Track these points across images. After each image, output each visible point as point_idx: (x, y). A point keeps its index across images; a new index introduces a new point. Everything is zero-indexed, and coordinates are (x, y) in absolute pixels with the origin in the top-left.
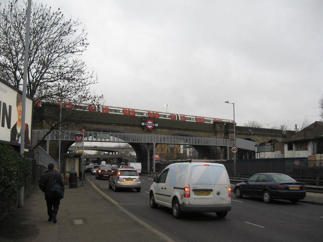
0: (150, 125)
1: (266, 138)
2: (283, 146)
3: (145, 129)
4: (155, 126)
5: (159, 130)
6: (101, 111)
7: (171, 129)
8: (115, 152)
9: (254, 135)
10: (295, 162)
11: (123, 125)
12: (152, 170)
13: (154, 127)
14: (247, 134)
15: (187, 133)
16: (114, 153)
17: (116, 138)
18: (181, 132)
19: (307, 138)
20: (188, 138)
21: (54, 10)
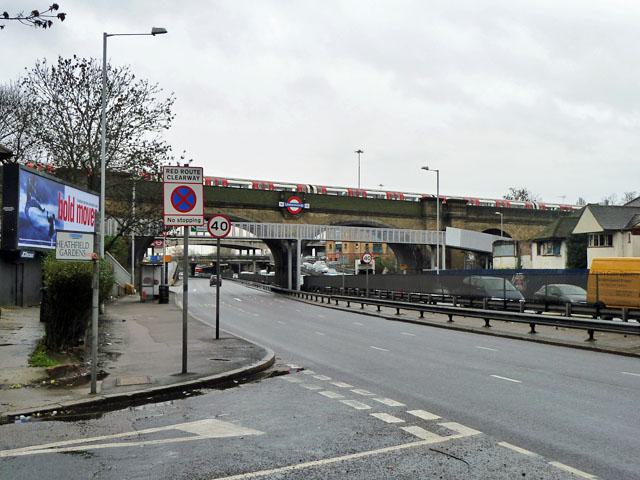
0: (294, 205)
1: (535, 227)
2: (36, 306)
3: (287, 214)
4: (303, 208)
5: (312, 214)
6: (316, 192)
7: (334, 212)
8: (254, 249)
9: (506, 221)
10: (585, 298)
11: (246, 206)
12: (294, 287)
13: (303, 211)
14: (490, 221)
15: (365, 219)
16: (251, 251)
17: (244, 231)
18: (355, 218)
19: (558, 235)
20: (382, 230)
21: (624, 196)
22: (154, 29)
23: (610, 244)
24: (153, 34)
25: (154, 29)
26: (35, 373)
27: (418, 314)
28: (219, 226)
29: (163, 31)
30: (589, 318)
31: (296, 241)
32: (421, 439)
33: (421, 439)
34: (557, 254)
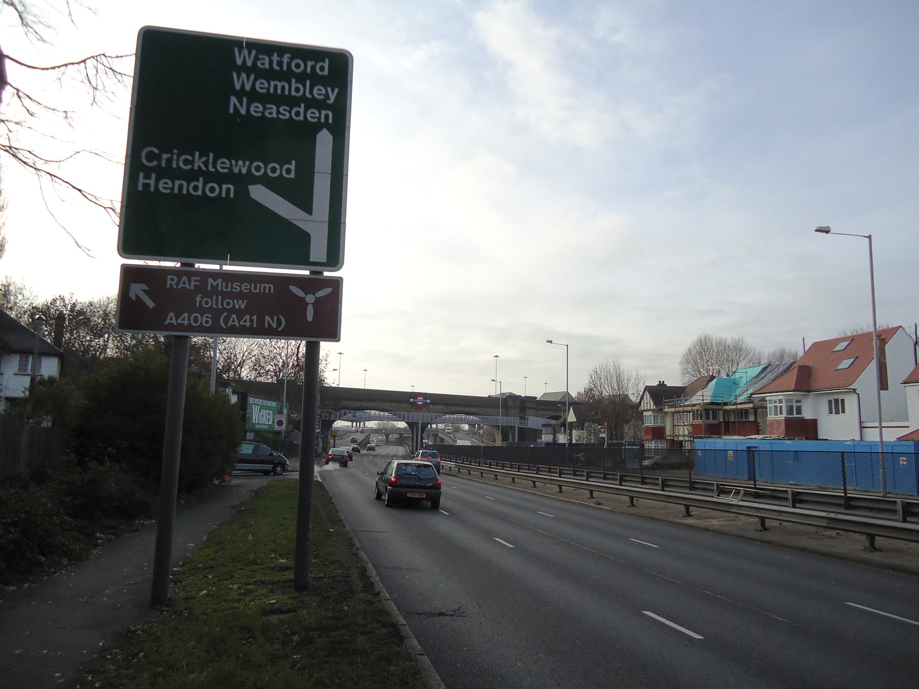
31: (418, 423)
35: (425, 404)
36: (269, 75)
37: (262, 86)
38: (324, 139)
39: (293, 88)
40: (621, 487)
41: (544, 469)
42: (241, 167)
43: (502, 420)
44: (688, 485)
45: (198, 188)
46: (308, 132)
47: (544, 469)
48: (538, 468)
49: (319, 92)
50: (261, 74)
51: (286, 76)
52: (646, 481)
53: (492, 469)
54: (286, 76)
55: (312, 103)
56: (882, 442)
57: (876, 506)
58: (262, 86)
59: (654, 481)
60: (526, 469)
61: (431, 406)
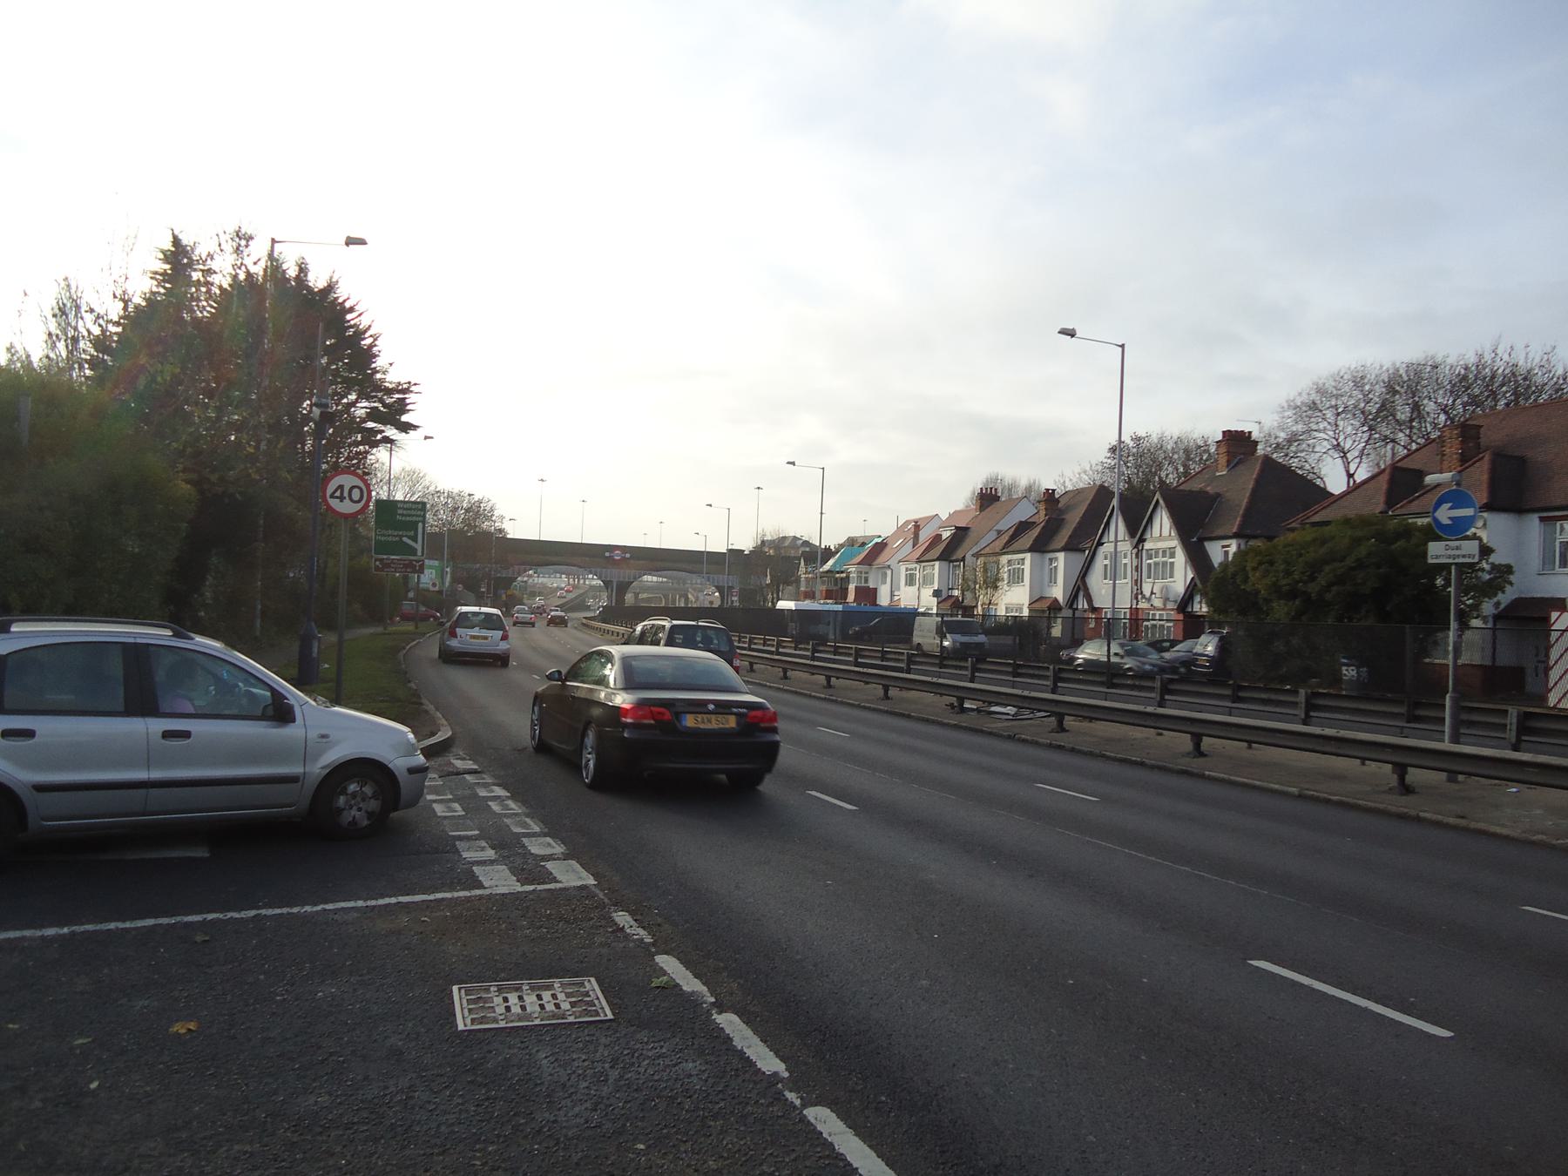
22: (348, 238)
23: (1224, 432)
24: (347, 244)
25: (348, 238)
26: (1126, 438)
27: (1184, 741)
28: (346, 494)
29: (362, 242)
30: (1230, 704)
31: (611, 581)
32: (560, 882)
33: (560, 882)
34: (1056, 559)
35: (624, 559)
36: (407, 509)
37: (405, 512)
38: (420, 525)
39: (413, 512)
40: (1161, 711)
41: (844, 651)
42: (401, 533)
43: (724, 580)
44: (937, 662)
45: (390, 539)
46: (417, 522)
47: (867, 654)
48: (883, 652)
49: (419, 513)
50: (404, 509)
51: (410, 509)
52: (1019, 671)
53: (816, 663)
54: (410, 509)
55: (417, 516)
56: (1114, 608)
57: (1036, 672)
58: (405, 512)
59: (1041, 673)
60: (761, 644)
61: (632, 561)
